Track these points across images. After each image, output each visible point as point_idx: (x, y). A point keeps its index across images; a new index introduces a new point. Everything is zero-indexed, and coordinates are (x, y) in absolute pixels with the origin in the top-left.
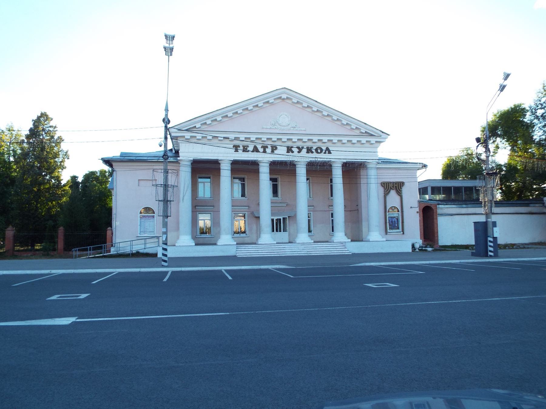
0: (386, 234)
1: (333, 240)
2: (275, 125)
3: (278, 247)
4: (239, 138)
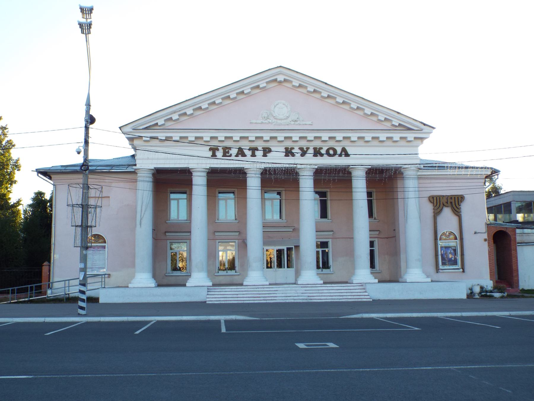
0: (437, 272)
1: (353, 280)
2: (268, 118)
3: (268, 289)
4: (171, 137)
